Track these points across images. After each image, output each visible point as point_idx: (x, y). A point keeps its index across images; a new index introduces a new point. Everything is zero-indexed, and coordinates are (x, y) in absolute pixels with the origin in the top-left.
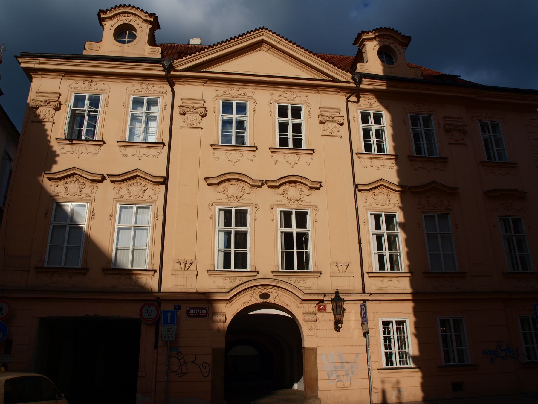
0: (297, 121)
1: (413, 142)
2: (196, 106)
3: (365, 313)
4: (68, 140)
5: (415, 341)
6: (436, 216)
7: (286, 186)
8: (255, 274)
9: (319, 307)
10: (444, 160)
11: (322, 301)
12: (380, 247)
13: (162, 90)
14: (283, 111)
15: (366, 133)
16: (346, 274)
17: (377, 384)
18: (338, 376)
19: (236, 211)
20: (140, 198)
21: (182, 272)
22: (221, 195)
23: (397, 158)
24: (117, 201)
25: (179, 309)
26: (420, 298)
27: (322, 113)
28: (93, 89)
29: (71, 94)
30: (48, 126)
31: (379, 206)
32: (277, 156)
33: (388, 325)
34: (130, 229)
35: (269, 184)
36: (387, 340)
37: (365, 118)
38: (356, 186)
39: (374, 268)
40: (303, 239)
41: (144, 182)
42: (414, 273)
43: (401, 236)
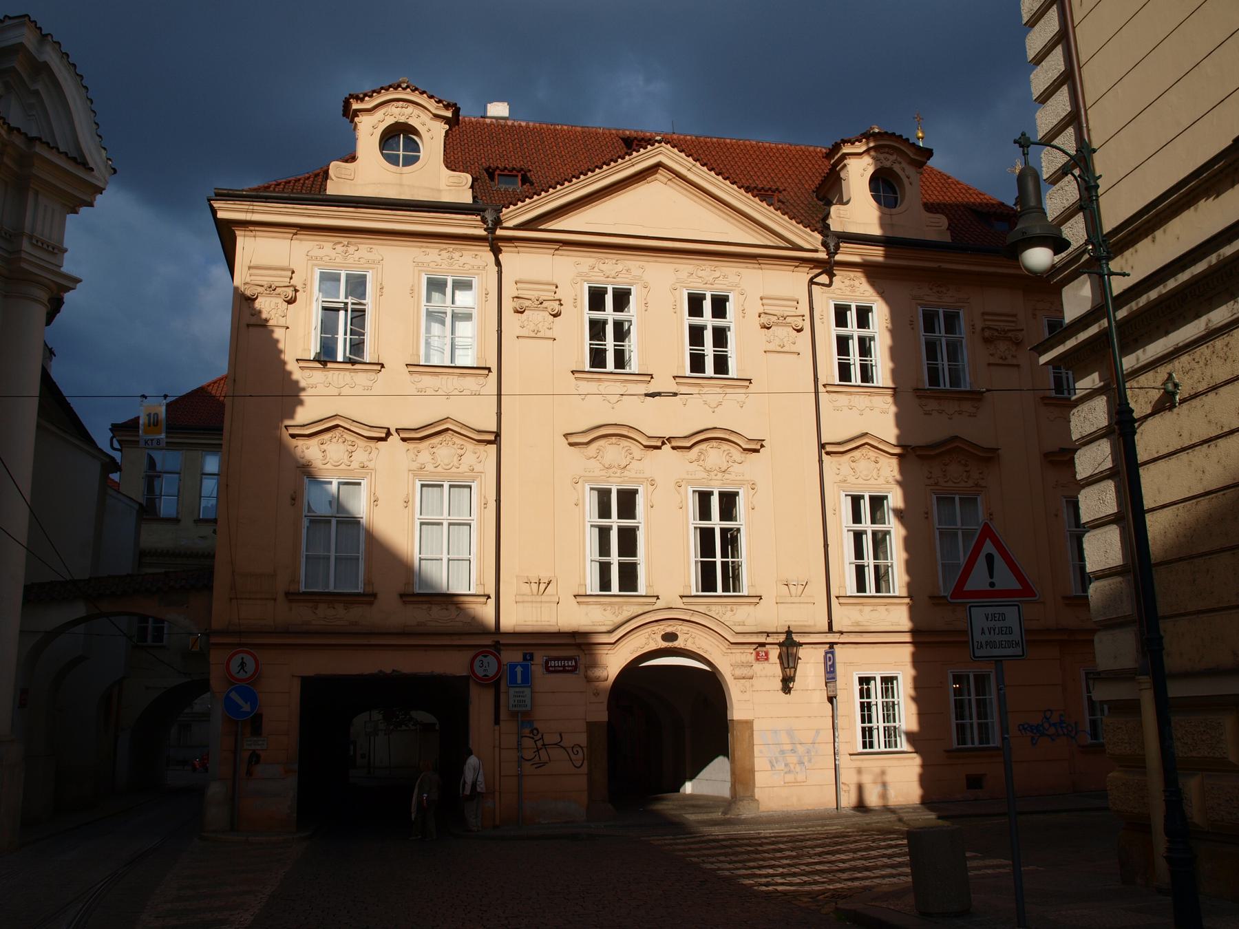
0: (719, 322)
1: (925, 362)
2: (277, 281)
3: (833, 665)
4: (319, 361)
5: (913, 708)
6: (957, 498)
7: (703, 446)
8: (654, 600)
9: (758, 654)
10: (976, 396)
11: (762, 645)
12: (859, 553)
13: (478, 262)
14: (695, 304)
15: (843, 343)
16: (802, 599)
17: (849, 778)
18: (786, 765)
19: (620, 492)
20: (454, 470)
21: (534, 599)
22: (593, 464)
23: (896, 392)
24: (415, 475)
25: (532, 659)
26: (926, 641)
27: (768, 309)
28: (351, 261)
29: (419, 275)
30: (278, 334)
31: (860, 481)
32: (585, 387)
33: (868, 684)
34: (441, 524)
35: (674, 444)
36: (866, 708)
37: (841, 315)
38: (822, 446)
39: (589, 587)
40: (731, 540)
41: (458, 440)
42: (921, 599)
43: (896, 532)
